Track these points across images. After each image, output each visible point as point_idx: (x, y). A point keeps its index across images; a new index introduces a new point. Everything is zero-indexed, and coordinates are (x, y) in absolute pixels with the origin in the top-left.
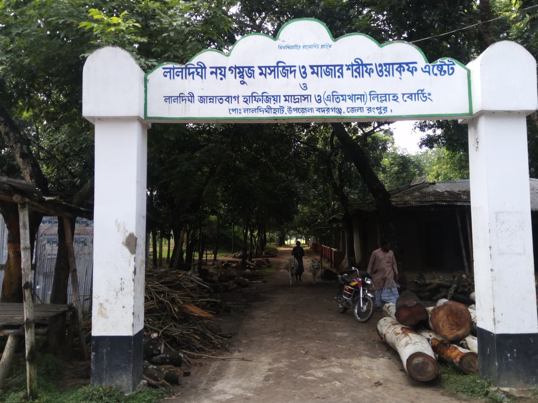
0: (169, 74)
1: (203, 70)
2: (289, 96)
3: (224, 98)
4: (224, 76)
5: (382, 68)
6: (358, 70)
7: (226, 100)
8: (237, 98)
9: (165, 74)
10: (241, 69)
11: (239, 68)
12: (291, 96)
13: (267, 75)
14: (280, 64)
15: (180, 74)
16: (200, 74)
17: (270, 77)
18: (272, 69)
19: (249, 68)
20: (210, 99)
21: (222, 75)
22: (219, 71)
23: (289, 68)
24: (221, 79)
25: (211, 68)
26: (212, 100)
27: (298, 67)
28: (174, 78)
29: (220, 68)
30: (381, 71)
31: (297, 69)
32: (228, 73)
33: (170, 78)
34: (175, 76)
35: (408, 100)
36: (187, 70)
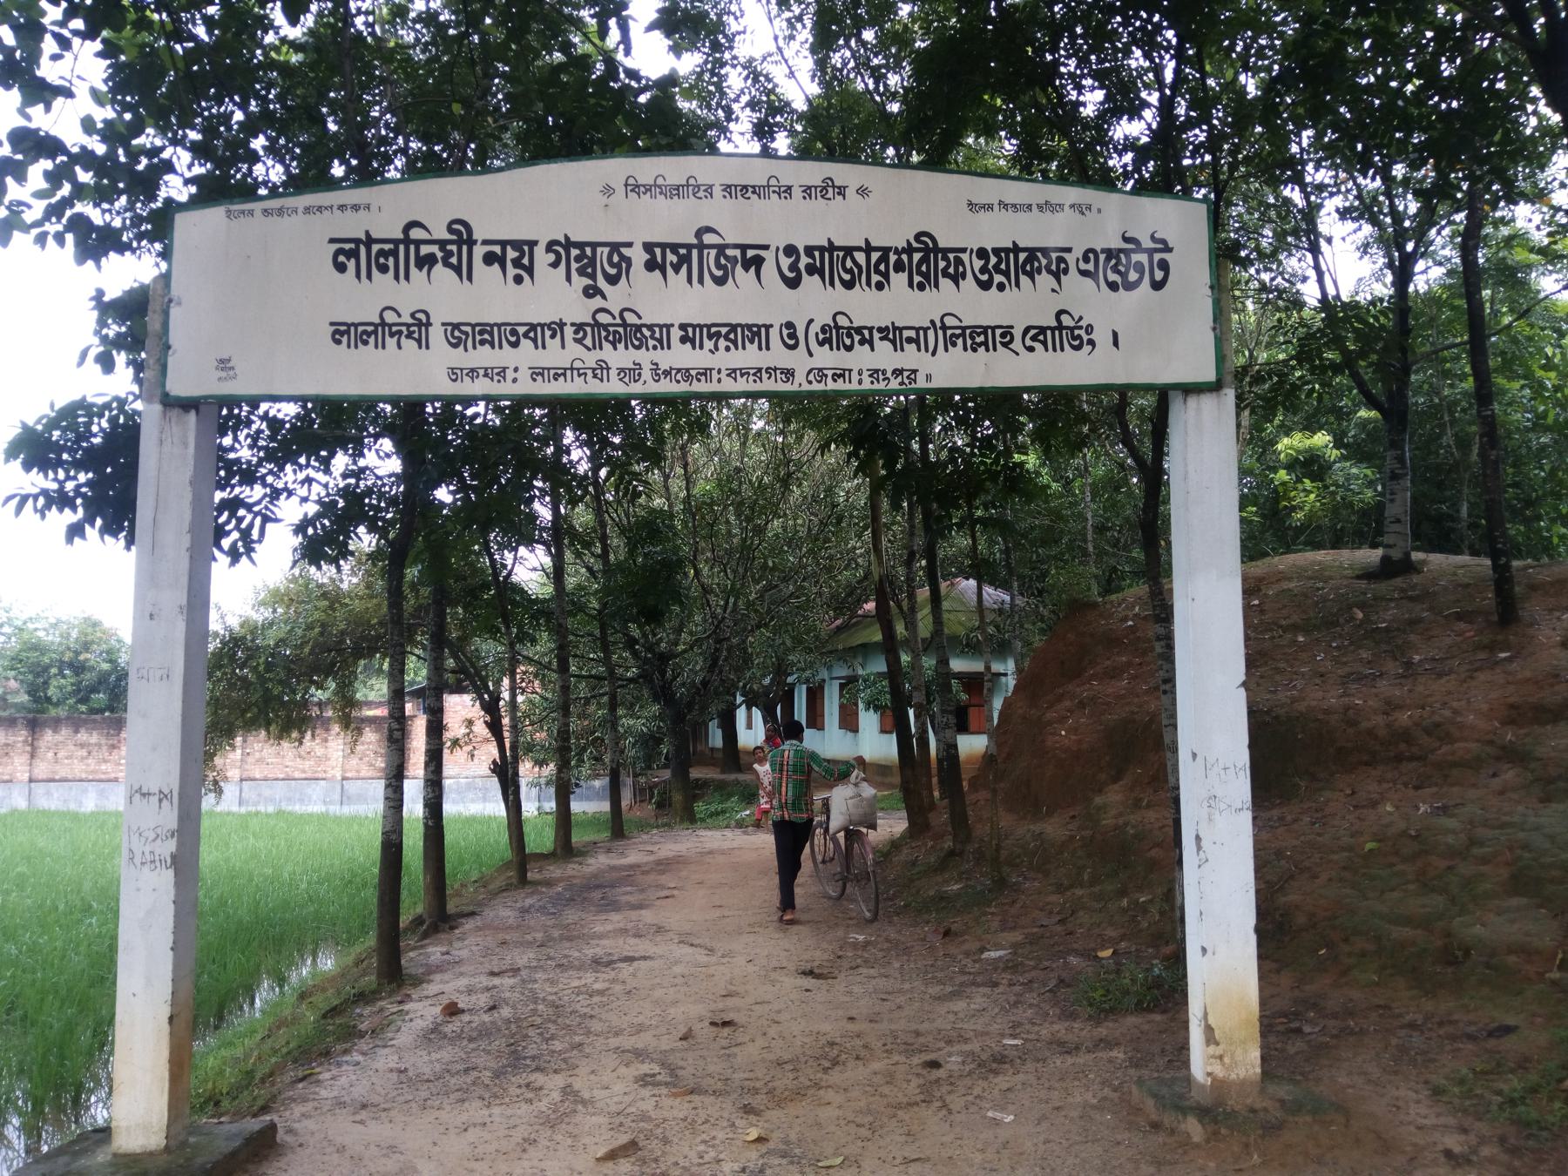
0: (391, 260)
1: (465, 248)
2: (694, 327)
3: (521, 330)
4: (530, 270)
5: (798, 260)
6: (882, 267)
7: (526, 335)
8: (557, 328)
9: (342, 258)
10: (588, 251)
11: (581, 245)
12: (701, 327)
13: (669, 270)
14: (709, 239)
15: (391, 261)
16: (454, 260)
17: (677, 280)
18: (683, 251)
19: (615, 247)
20: (481, 333)
21: (523, 267)
22: (511, 254)
23: (737, 253)
24: (518, 280)
25: (485, 242)
26: (486, 336)
27: (773, 249)
28: (369, 277)
29: (517, 245)
30: (984, 270)
31: (768, 256)
32: (542, 258)
33: (358, 276)
34: (413, 270)
35: (1037, 345)
36: (412, 248)
